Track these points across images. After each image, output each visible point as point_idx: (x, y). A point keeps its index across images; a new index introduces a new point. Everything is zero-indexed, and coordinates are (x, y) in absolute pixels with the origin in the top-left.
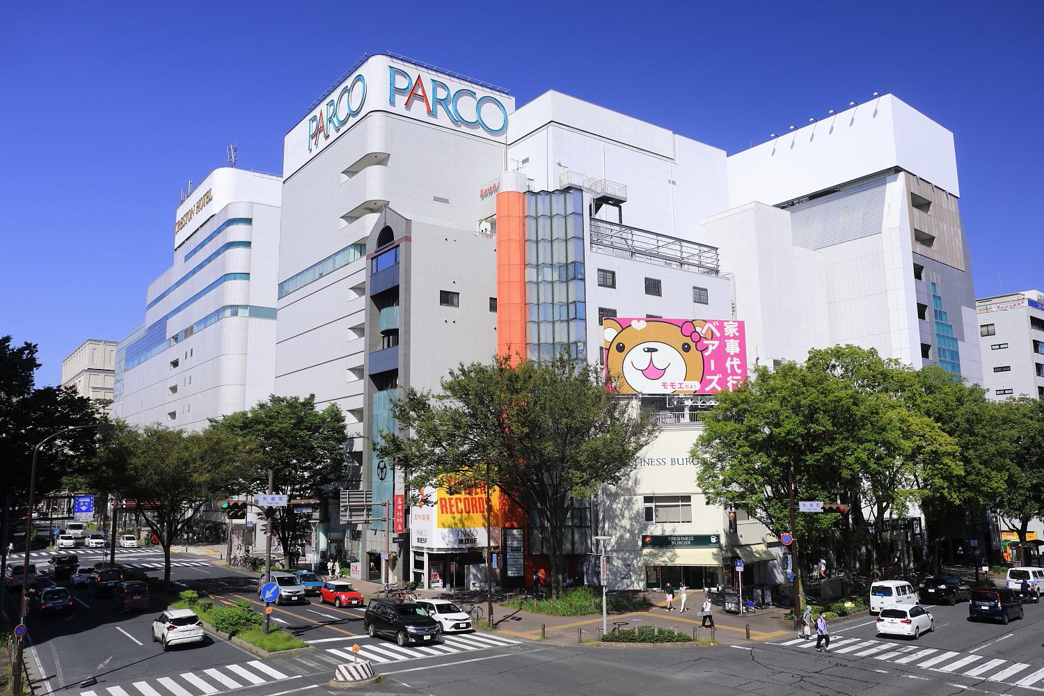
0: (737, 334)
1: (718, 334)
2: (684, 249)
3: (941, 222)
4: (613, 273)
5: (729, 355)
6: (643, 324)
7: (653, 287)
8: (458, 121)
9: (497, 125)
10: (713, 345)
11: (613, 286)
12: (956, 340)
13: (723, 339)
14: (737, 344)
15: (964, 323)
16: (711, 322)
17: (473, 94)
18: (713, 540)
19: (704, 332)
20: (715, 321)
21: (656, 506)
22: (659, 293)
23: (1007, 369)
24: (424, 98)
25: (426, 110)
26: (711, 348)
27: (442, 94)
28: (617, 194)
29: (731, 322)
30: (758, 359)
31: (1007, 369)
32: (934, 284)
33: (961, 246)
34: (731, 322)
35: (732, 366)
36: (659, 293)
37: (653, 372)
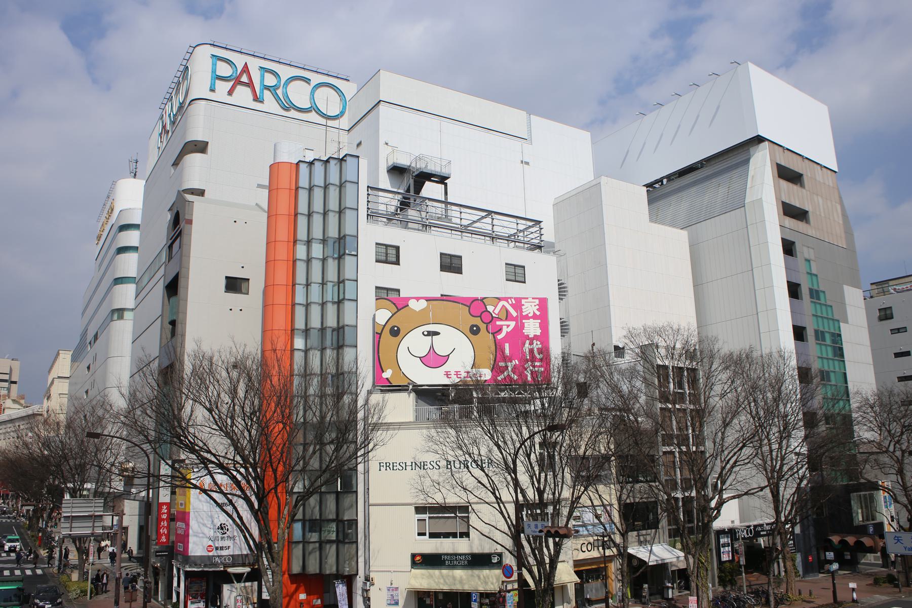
0: (538, 313)
1: (514, 314)
2: (463, 216)
3: (815, 197)
4: (397, 249)
5: (527, 337)
6: (423, 304)
7: (451, 264)
8: (288, 106)
9: (334, 111)
10: (508, 327)
11: (397, 262)
12: (838, 321)
13: (521, 318)
14: (538, 325)
15: (847, 302)
16: (506, 299)
17: (307, 81)
18: (495, 560)
19: (497, 311)
20: (510, 298)
21: (430, 518)
22: (459, 270)
23: (897, 355)
24: (250, 84)
25: (251, 97)
26: (505, 330)
27: (270, 80)
28: (443, 171)
29: (530, 300)
30: (594, 344)
31: (897, 355)
32: (808, 261)
33: (841, 222)
34: (530, 300)
35: (531, 351)
36: (459, 270)
37: (433, 360)
